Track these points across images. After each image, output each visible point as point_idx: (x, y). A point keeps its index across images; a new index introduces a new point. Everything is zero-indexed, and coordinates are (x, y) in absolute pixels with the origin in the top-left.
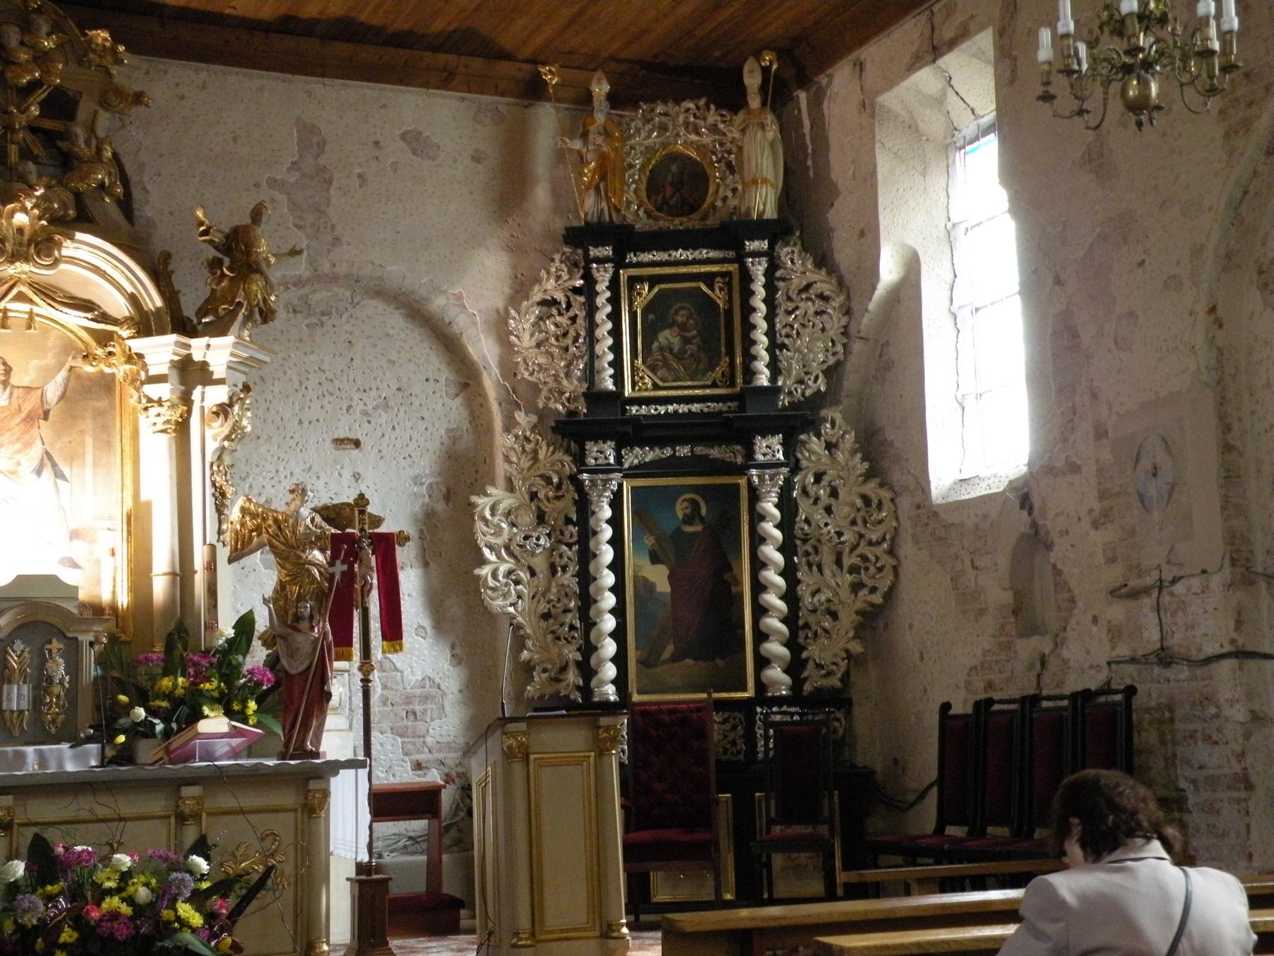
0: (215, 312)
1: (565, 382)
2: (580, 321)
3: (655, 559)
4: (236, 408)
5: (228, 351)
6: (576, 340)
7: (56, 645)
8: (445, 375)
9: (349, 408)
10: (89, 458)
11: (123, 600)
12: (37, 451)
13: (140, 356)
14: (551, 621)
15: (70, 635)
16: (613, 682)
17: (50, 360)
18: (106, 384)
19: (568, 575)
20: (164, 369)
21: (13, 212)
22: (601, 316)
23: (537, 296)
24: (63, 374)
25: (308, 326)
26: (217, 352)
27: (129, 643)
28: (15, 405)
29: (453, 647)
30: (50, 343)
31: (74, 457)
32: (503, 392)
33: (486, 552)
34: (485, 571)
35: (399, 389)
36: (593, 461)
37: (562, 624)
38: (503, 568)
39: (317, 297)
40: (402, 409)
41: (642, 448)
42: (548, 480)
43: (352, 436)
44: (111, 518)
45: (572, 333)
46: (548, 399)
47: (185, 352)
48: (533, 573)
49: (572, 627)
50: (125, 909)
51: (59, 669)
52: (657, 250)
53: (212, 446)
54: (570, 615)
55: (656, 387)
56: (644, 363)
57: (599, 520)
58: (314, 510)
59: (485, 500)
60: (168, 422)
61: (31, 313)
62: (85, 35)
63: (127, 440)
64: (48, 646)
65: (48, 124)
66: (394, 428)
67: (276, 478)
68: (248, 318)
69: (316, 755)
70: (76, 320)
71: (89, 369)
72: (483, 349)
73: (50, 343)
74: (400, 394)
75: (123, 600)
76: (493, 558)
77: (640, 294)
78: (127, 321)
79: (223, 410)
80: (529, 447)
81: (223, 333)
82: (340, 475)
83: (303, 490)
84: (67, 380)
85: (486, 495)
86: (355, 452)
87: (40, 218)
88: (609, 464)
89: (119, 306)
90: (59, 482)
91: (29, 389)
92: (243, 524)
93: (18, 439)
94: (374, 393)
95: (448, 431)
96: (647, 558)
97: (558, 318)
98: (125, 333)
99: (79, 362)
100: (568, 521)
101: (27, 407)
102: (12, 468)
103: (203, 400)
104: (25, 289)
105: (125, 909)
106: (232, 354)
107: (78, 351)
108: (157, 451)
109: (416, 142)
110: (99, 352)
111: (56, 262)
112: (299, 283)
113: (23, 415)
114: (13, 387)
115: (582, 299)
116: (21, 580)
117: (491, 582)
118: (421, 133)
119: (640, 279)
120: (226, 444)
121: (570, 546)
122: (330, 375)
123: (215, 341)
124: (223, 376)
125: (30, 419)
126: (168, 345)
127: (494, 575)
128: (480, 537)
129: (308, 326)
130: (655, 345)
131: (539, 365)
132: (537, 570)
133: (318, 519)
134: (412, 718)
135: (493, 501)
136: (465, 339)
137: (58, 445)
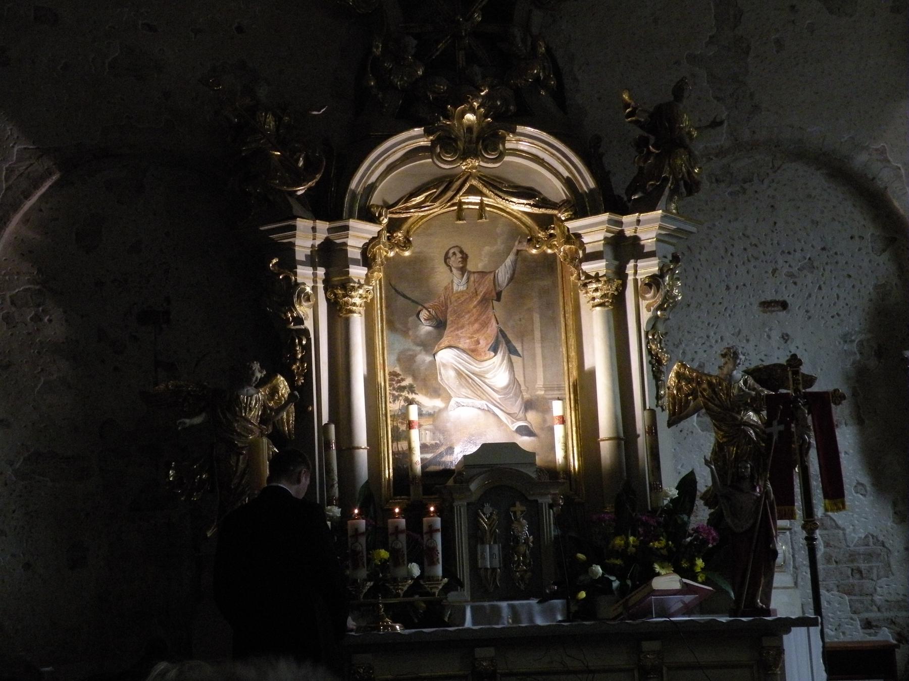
5: (657, 225)
7: (519, 508)
8: (870, 231)
9: (774, 271)
10: (537, 334)
15: (531, 498)
17: (499, 246)
18: (549, 264)
20: (600, 247)
25: (731, 194)
26: (646, 227)
28: (472, 290)
29: (895, 504)
30: (498, 230)
31: (524, 334)
35: (823, 249)
40: (828, 268)
43: (779, 298)
44: (560, 388)
51: (524, 530)
53: (646, 316)
60: (604, 296)
64: (512, 509)
66: (820, 288)
67: (708, 344)
68: (675, 191)
70: (519, 206)
79: (654, 281)
81: (653, 209)
84: (515, 263)
86: (782, 314)
89: (557, 190)
90: (514, 357)
91: (483, 274)
92: (679, 389)
93: (476, 320)
94: (798, 255)
95: (876, 287)
99: (524, 246)
101: (482, 290)
103: (636, 273)
106: (661, 228)
110: (541, 235)
113: (479, 298)
114: (470, 272)
122: (754, 241)
123: (644, 216)
124: (654, 249)
125: (485, 301)
129: (731, 194)
133: (751, 381)
134: (858, 576)
136: (889, 193)
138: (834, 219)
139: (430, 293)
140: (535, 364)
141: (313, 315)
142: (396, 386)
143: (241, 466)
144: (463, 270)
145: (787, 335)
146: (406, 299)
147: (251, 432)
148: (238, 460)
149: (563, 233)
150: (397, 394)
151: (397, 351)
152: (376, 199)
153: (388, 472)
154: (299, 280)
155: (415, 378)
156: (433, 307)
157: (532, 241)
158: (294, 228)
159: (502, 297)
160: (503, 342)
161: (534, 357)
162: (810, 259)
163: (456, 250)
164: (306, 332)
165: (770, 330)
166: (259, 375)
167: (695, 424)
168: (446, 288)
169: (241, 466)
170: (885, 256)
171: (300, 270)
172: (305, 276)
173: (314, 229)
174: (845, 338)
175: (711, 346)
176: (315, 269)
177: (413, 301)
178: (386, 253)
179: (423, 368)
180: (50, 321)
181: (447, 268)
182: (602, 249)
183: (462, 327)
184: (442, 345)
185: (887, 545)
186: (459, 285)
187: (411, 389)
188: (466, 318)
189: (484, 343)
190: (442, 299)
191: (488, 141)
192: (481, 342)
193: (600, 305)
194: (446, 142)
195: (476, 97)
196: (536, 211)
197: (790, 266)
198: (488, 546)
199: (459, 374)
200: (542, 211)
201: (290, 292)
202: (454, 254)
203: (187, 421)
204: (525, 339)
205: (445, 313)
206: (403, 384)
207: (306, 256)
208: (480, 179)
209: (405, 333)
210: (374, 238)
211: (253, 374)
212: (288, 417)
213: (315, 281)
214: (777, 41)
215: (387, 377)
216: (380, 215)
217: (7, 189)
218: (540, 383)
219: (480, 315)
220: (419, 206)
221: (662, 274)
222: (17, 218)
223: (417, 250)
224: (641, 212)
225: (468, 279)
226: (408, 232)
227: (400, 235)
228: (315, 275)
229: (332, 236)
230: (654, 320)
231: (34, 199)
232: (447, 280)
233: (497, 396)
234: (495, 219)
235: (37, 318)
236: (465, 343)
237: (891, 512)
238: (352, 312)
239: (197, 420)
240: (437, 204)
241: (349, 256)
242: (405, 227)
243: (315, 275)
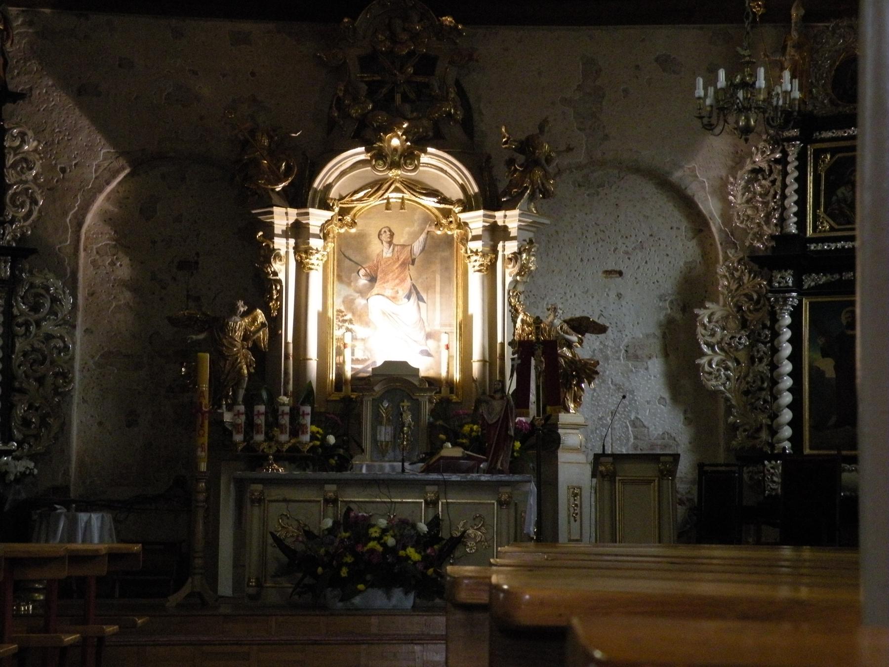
0: (510, 195)
1: (765, 227)
2: (778, 183)
3: (825, 355)
4: (524, 256)
5: (517, 218)
6: (774, 197)
7: (406, 404)
8: (684, 224)
9: (616, 249)
10: (438, 288)
11: (457, 377)
12: (408, 283)
13: (466, 224)
14: (750, 396)
15: (415, 398)
16: (789, 440)
17: (416, 227)
18: (448, 241)
19: (763, 364)
20: (479, 232)
21: (391, 138)
22: (790, 179)
23: (749, 166)
24: (422, 238)
26: (511, 219)
27: (461, 403)
28: (396, 256)
29: (685, 412)
30: (416, 217)
31: (429, 288)
32: (724, 235)
33: (705, 348)
34: (704, 361)
35: (651, 235)
36: (777, 285)
37: (759, 399)
38: (716, 359)
39: (596, 175)
40: (653, 249)
41: (817, 274)
42: (750, 298)
43: (617, 269)
44: (450, 325)
45: (772, 192)
46: (752, 240)
47: (492, 220)
48: (738, 363)
49: (765, 401)
50: (380, 548)
51: (408, 418)
52: (836, 129)
53: (509, 279)
54: (764, 393)
55: (832, 229)
56: (825, 211)
57: (780, 327)
58: (565, 321)
59: (705, 311)
60: (481, 265)
61: (403, 199)
62: (439, 20)
63: (460, 277)
64: (402, 404)
65: (419, 79)
66: (646, 262)
68: (532, 197)
70: (431, 203)
71: (439, 233)
72: (710, 206)
73: (416, 217)
74: (652, 239)
75: (457, 377)
76: (710, 352)
77: (823, 161)
78: (459, 202)
79: (516, 257)
80: (737, 274)
81: (514, 208)
82: (608, 295)
83: (555, 308)
84: (426, 239)
85: (706, 308)
86: (619, 280)
87: (406, 140)
88: (788, 286)
89: (456, 193)
90: (421, 303)
91: (403, 246)
92: (523, 330)
93: (397, 278)
94: (633, 239)
95: (686, 263)
96: (820, 354)
97: (763, 182)
98: (457, 209)
99: (433, 229)
100: (764, 326)
101: (402, 258)
102: (393, 295)
103: (504, 250)
104: (398, 185)
105: (380, 548)
106: (519, 221)
107: (432, 221)
108: (475, 281)
109: (665, 62)
110: (444, 221)
111: (416, 168)
112: (580, 167)
114: (395, 245)
115: (779, 167)
116: (387, 364)
117: (707, 368)
118: (670, 56)
119: (825, 151)
120: (518, 278)
121: (765, 344)
122: (603, 228)
123: (508, 213)
124: (516, 234)
125: (404, 265)
126: (479, 216)
127: (710, 365)
128: (699, 336)
129: (588, 195)
130: (834, 198)
131: (748, 216)
132: (741, 361)
133: (565, 327)
135: (710, 314)
136: (696, 199)
137: (420, 280)
138: (659, 215)
139: (367, 258)
141: (284, 269)
142: (341, 319)
143: (228, 367)
144: (390, 243)
146: (350, 261)
147: (235, 346)
148: (225, 365)
149: (456, 220)
152: (333, 193)
153: (332, 376)
154: (276, 247)
155: (353, 314)
156: (369, 267)
157: (438, 225)
158: (272, 213)
160: (414, 292)
161: (434, 304)
163: (386, 230)
164: (280, 281)
166: (242, 309)
168: (378, 255)
169: (228, 367)
170: (694, 243)
171: (276, 240)
172: (279, 244)
173: (287, 213)
174: (661, 298)
176: (287, 239)
177: (356, 263)
178: (336, 229)
179: (359, 308)
180: (121, 265)
182: (481, 233)
183: (388, 281)
185: (677, 439)
186: (387, 253)
187: (351, 321)
188: (390, 276)
189: (403, 291)
191: (409, 156)
193: (480, 271)
194: (379, 156)
195: (400, 128)
196: (438, 205)
200: (442, 206)
201: (269, 254)
203: (194, 337)
205: (376, 272)
206: (345, 318)
207: (283, 231)
208: (402, 182)
209: (349, 284)
210: (329, 220)
211: (238, 308)
212: (263, 335)
213: (287, 248)
214: (625, 91)
215: (335, 313)
216: (333, 205)
217: (96, 178)
219: (400, 274)
220: (360, 200)
221: (520, 253)
222: (101, 198)
223: (360, 228)
224: (506, 210)
226: (355, 215)
227: (348, 218)
228: (287, 244)
229: (300, 218)
230: (515, 283)
231: (114, 184)
232: (378, 249)
234: (414, 210)
235: (113, 264)
236: (389, 292)
237: (682, 417)
238: (311, 269)
239: (201, 336)
240: (372, 199)
241: (311, 231)
242: (352, 213)
243: (287, 244)
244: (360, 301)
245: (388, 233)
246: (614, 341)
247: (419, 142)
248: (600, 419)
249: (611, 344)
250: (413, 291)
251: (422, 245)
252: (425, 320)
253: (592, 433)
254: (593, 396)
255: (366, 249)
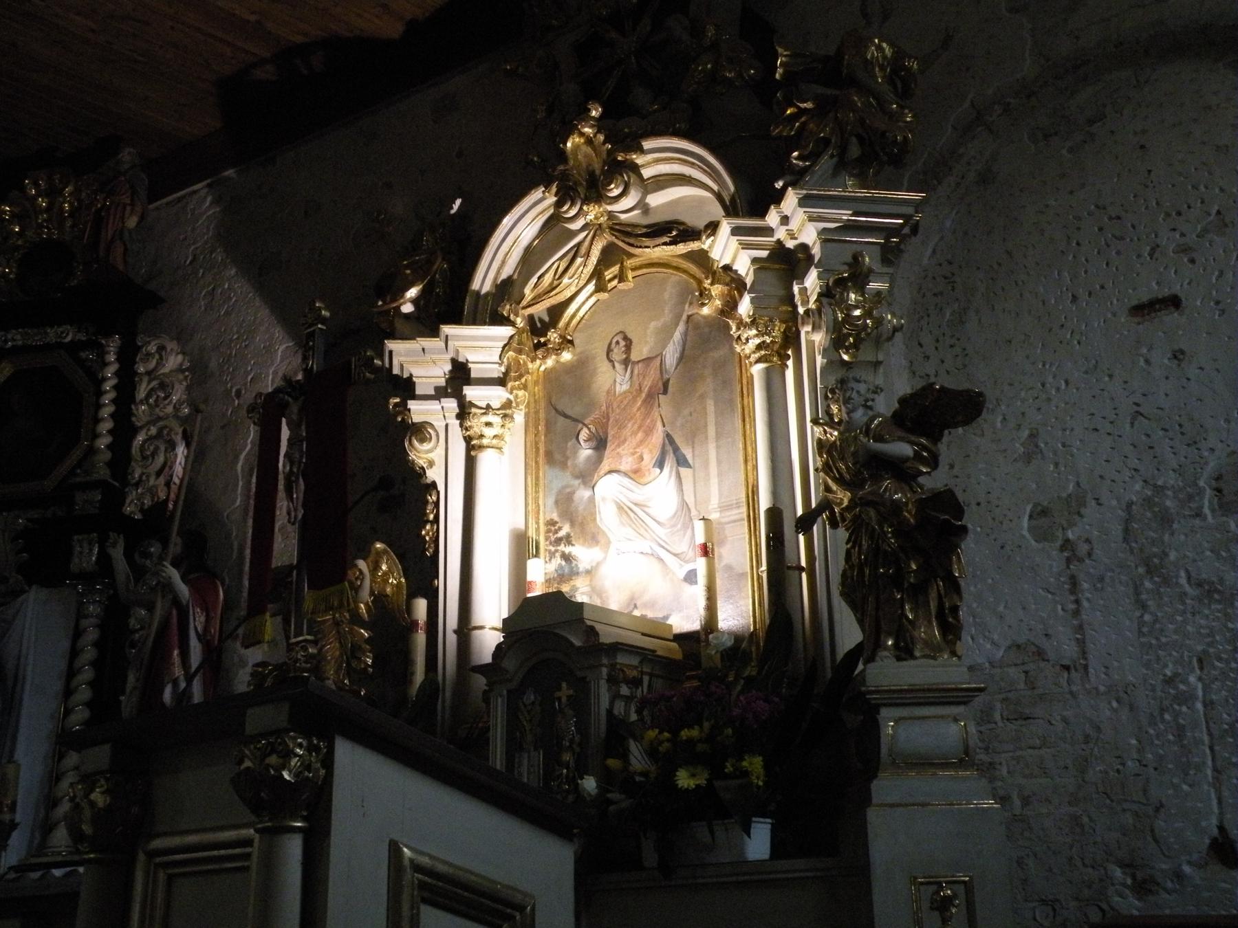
12: (658, 436)
15: (579, 674)
17: (667, 316)
24: (681, 328)
28: (637, 386)
30: (666, 296)
31: (696, 433)
43: (1166, 292)
60: (759, 347)
64: (558, 694)
69: (582, 778)
82: (1147, 361)
86: (1171, 318)
90: (683, 470)
91: (648, 360)
101: (647, 384)
113: (644, 395)
125: (651, 398)
129: (1071, 150)
139: (591, 405)
140: (708, 475)
141: (440, 458)
144: (626, 362)
145: (1182, 352)
150: (553, 549)
151: (554, 492)
155: (572, 524)
159: (670, 389)
160: (672, 453)
161: (706, 465)
162: (1219, 212)
163: (619, 338)
164: (434, 485)
165: (1150, 349)
167: (1025, 533)
168: (608, 392)
175: (1049, 400)
179: (581, 508)
181: (609, 365)
184: (602, 472)
188: (627, 432)
189: (649, 458)
190: (604, 408)
192: (646, 457)
197: (1183, 235)
198: (526, 755)
199: (620, 508)
202: (618, 343)
204: (696, 440)
209: (563, 465)
215: (543, 528)
218: (714, 501)
225: (632, 372)
232: (611, 381)
233: (662, 532)
244: (583, 494)
245: (623, 343)
246: (1180, 471)
247: (624, 135)
248: (1169, 681)
249: (1171, 479)
250: (669, 448)
251: (679, 349)
252: (692, 505)
253: (1152, 723)
254: (1141, 623)
255: (589, 387)
